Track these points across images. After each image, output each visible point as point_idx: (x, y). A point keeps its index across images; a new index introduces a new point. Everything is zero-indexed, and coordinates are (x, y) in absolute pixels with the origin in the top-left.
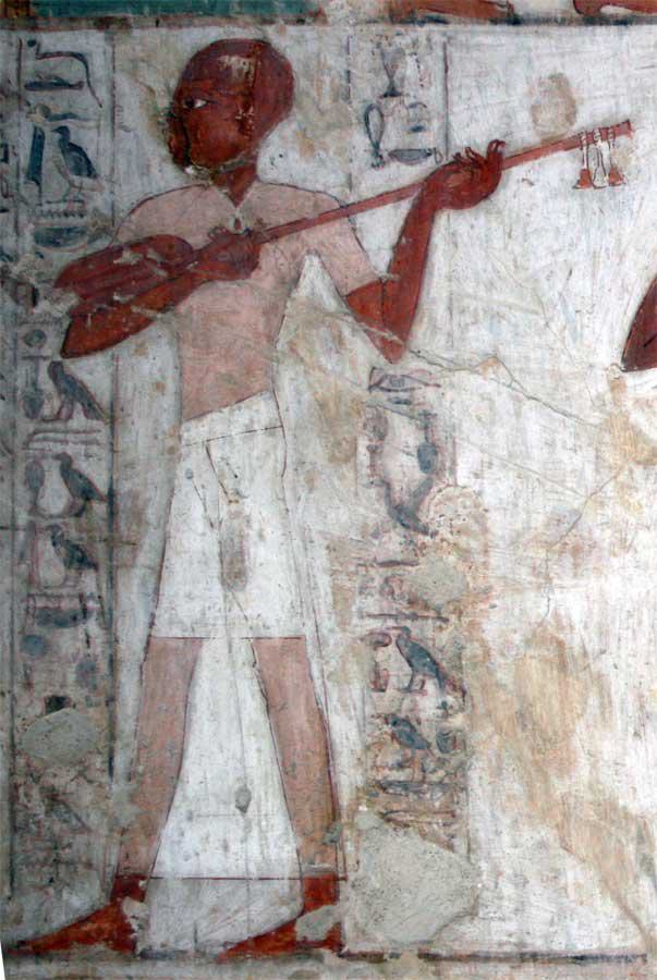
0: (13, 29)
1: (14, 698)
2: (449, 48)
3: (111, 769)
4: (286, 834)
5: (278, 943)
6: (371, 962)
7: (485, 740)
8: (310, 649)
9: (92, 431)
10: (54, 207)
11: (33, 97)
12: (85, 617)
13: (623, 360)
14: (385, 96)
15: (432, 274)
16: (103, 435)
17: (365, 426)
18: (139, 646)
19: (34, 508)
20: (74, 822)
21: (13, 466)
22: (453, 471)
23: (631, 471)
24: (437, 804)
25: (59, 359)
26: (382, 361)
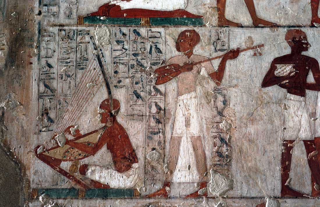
0: (146, 27)
1: (145, 148)
2: (230, 32)
3: (164, 162)
4: (197, 174)
5: (195, 195)
6: (212, 199)
7: (234, 156)
8: (202, 139)
9: (161, 98)
10: (154, 59)
11: (150, 39)
12: (159, 133)
13: (262, 86)
14: (217, 40)
15: (226, 71)
16: (163, 99)
17: (213, 97)
18: (170, 138)
19: (150, 112)
20: (157, 172)
21: (146, 104)
22: (229, 105)
23: (263, 105)
24: (226, 168)
25: (155, 85)
26: (216, 85)
